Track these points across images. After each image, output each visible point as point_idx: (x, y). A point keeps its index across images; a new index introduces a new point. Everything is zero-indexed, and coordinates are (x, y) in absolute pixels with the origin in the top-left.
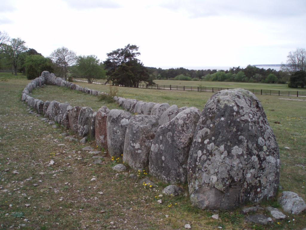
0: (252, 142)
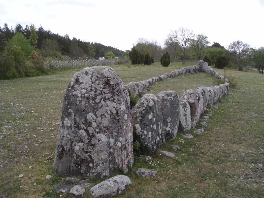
0: (80, 116)
